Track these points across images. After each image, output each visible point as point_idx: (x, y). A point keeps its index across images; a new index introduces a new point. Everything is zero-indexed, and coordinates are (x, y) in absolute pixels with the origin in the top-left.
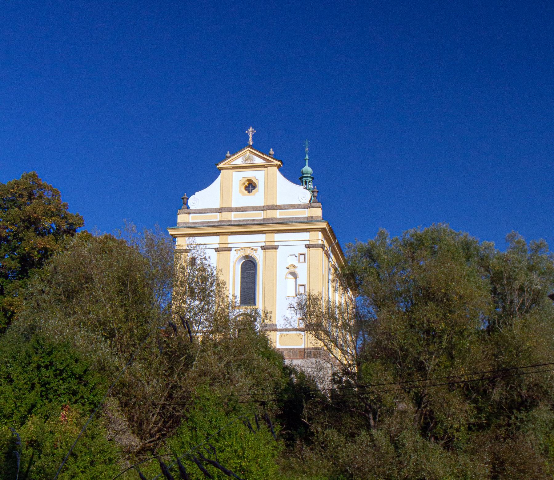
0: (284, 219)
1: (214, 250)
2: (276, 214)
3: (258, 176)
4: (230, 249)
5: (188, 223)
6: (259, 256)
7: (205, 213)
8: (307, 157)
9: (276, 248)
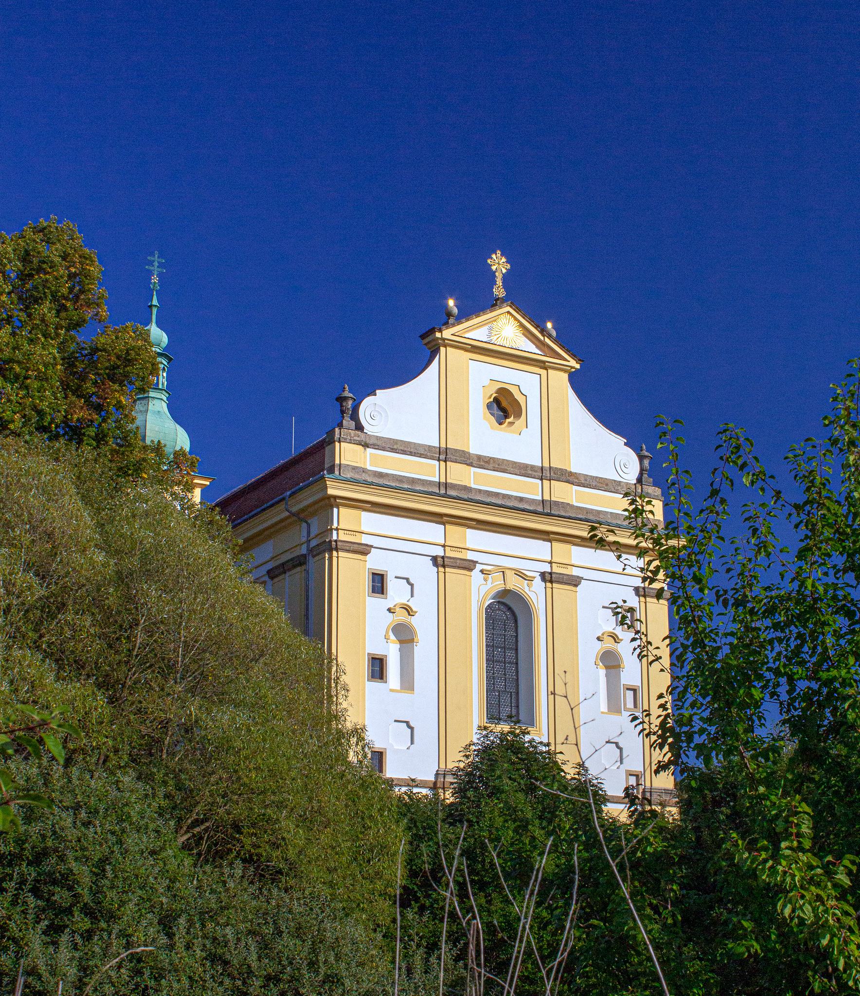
0: (588, 511)
1: (428, 562)
2: (365, 463)
3: (525, 383)
4: (468, 566)
5: (364, 471)
6: (535, 593)
7: (404, 452)
8: (155, 302)
9: (574, 582)
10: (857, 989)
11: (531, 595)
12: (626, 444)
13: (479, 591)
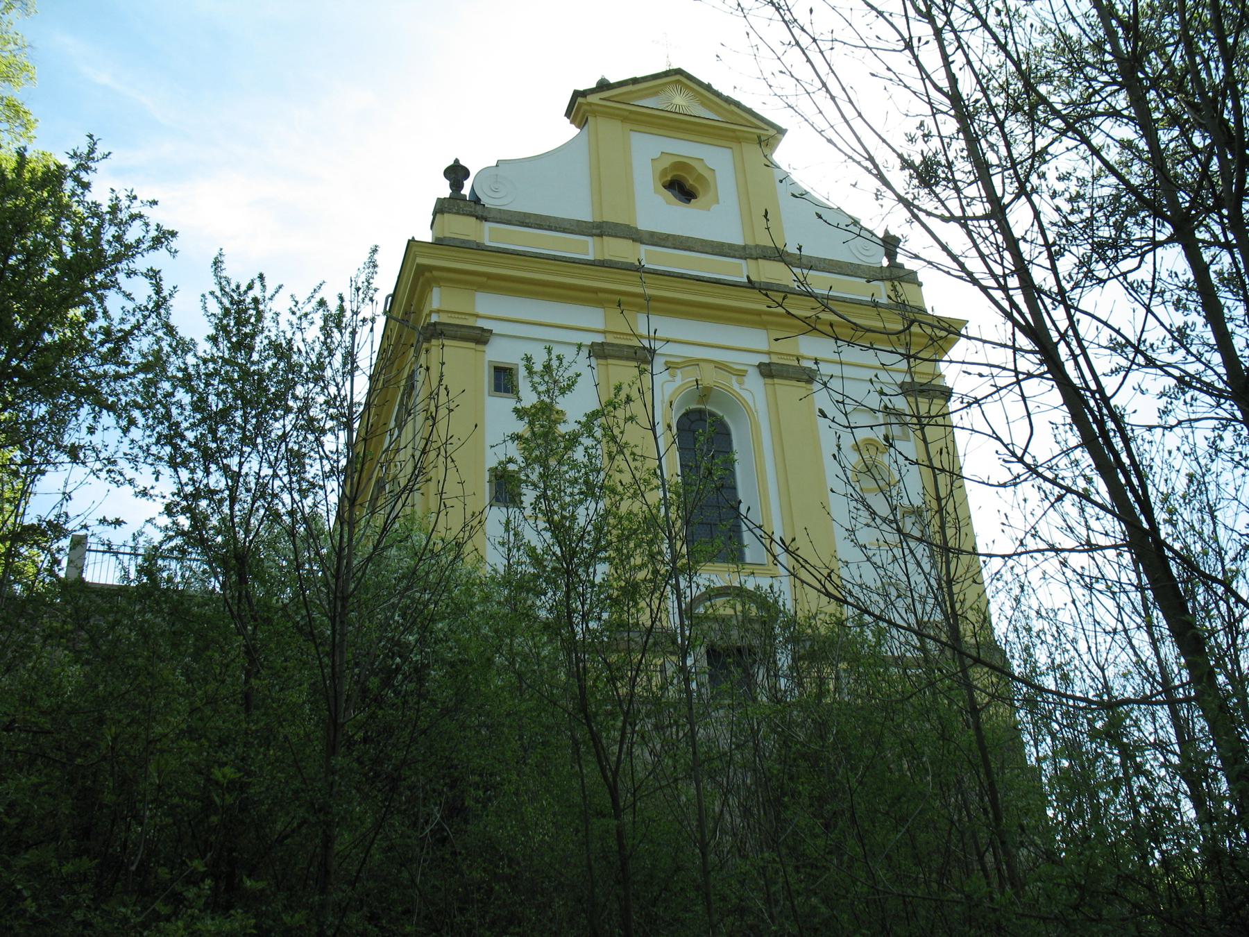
7: (540, 227)
10: (1245, 858)
11: (745, 394)
12: (412, 243)
13: (668, 392)
